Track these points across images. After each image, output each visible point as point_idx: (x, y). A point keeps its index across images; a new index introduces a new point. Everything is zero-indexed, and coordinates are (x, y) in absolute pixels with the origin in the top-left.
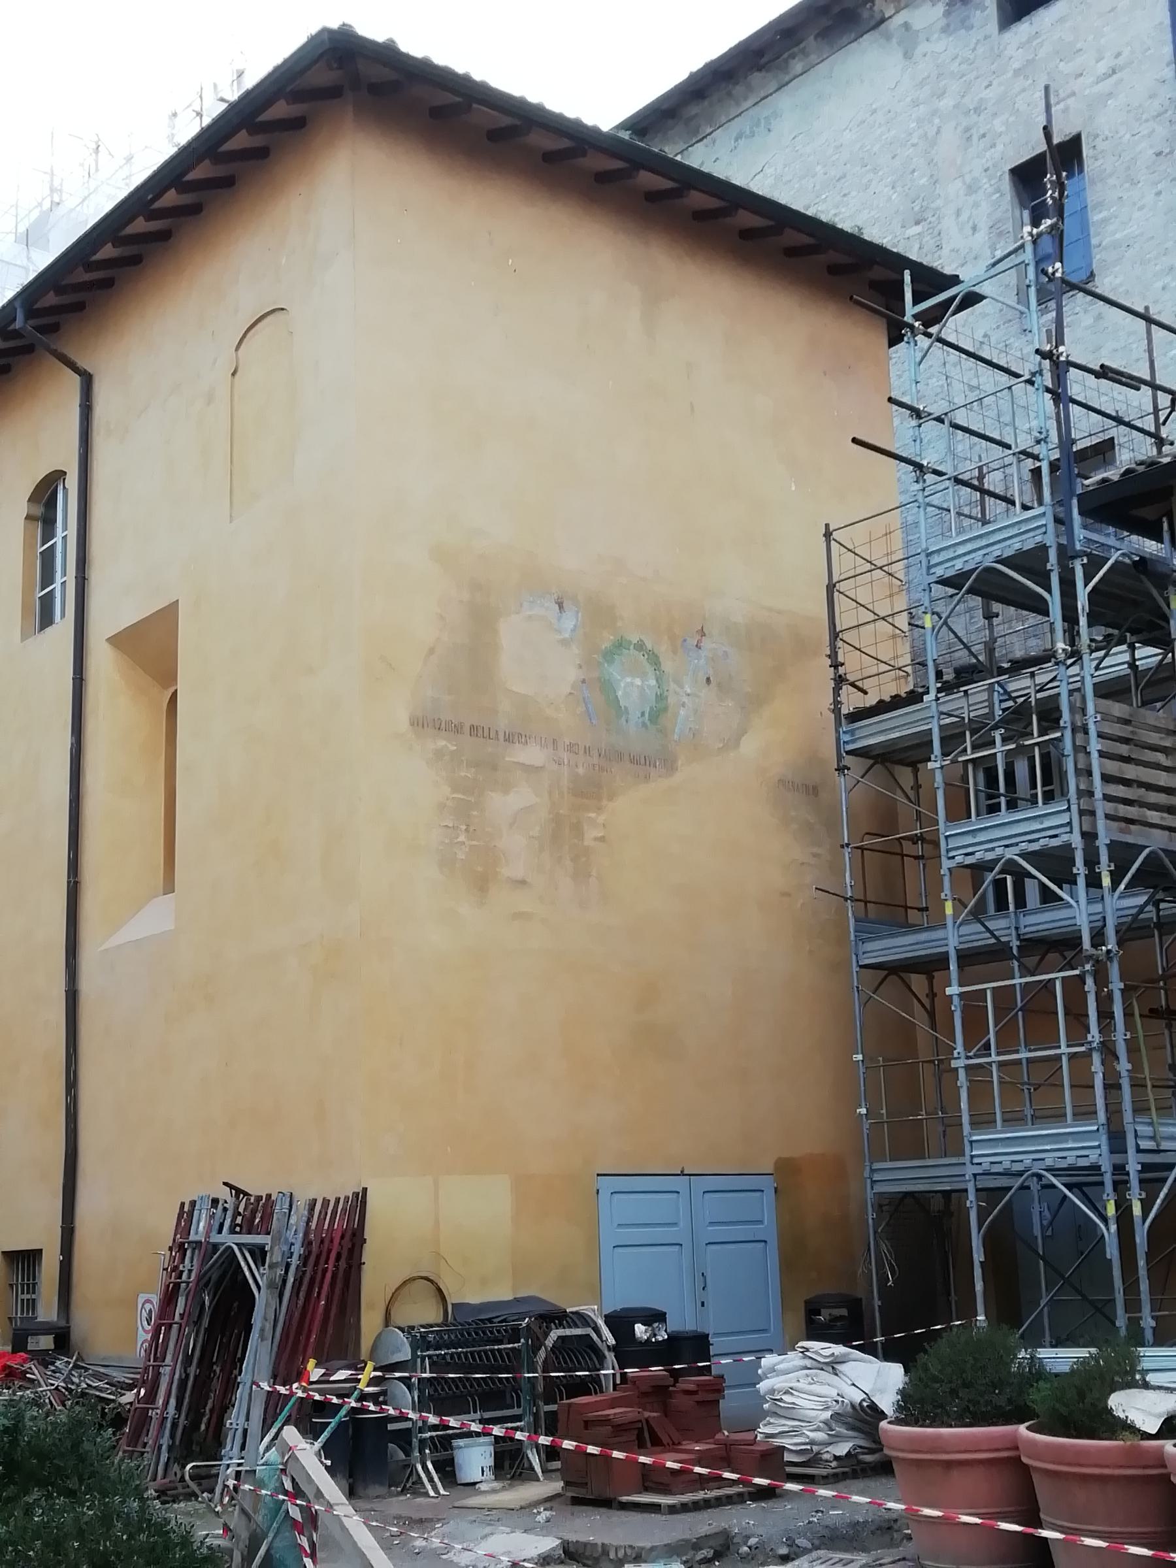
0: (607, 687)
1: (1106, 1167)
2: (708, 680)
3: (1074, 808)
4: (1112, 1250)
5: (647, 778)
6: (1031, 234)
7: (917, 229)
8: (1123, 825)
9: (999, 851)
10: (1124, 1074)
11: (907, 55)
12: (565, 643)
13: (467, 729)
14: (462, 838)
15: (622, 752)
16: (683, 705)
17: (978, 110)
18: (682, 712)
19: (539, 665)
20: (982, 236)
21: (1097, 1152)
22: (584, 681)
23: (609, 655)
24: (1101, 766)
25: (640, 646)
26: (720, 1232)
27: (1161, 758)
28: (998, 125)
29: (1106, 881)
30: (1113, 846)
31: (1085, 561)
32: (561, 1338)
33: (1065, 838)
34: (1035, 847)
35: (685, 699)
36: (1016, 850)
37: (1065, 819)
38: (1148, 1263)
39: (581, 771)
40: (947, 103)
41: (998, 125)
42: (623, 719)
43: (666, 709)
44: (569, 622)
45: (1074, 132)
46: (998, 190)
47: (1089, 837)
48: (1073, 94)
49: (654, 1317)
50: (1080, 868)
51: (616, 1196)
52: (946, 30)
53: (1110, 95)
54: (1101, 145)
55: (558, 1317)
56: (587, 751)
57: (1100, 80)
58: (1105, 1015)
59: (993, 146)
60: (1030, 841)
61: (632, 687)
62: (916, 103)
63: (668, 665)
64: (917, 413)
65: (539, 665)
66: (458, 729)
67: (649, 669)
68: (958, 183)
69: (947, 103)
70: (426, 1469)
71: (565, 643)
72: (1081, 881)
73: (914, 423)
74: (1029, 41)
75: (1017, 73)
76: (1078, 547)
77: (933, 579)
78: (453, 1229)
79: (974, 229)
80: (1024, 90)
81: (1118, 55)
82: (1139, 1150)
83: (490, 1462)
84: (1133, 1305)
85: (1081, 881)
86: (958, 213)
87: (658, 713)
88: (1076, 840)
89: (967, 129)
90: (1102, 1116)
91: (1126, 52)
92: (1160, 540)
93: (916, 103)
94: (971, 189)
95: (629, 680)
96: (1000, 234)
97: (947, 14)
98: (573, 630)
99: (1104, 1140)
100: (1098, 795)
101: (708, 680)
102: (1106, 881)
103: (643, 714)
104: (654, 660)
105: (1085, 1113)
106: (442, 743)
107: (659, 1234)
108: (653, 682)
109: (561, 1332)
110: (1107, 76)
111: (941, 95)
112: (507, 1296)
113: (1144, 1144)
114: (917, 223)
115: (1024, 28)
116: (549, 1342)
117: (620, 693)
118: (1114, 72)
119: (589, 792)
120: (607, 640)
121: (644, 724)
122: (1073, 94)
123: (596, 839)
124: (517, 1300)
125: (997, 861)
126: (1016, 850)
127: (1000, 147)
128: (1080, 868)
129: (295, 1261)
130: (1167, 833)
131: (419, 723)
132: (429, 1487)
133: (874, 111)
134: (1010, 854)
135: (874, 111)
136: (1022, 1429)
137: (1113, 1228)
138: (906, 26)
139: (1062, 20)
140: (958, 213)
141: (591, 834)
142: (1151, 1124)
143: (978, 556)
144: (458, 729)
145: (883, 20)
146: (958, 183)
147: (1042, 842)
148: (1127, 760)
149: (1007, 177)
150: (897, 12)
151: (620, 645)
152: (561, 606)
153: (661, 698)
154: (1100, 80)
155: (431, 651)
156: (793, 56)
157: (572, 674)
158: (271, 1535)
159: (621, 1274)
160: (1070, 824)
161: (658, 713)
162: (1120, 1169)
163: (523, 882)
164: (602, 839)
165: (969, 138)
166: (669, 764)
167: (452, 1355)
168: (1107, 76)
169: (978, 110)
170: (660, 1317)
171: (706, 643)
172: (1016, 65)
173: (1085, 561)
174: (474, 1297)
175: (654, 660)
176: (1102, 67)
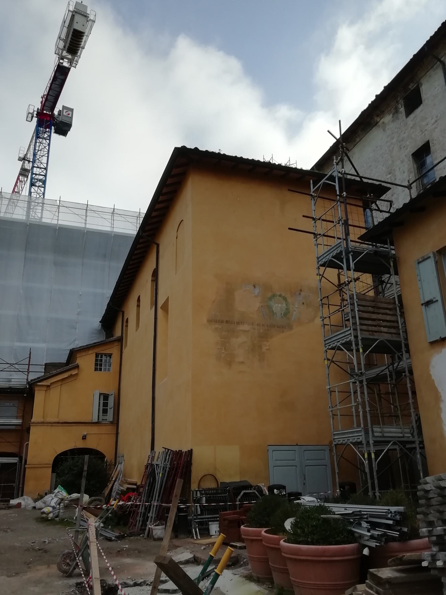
0: (270, 308)
1: (364, 442)
2: (303, 303)
3: (352, 329)
4: (367, 470)
5: (283, 332)
6: (336, 162)
7: (390, 175)
8: (371, 333)
9: (336, 344)
10: (368, 411)
11: (384, 130)
12: (256, 296)
13: (236, 323)
14: (223, 351)
15: (273, 325)
16: (295, 311)
17: (402, 140)
18: (295, 313)
19: (248, 303)
20: (406, 174)
21: (362, 438)
22: (262, 306)
23: (270, 299)
24: (359, 314)
25: (280, 296)
26: (279, 463)
27: (388, 312)
28: (408, 143)
29: (361, 350)
30: (363, 339)
31: (352, 253)
32: (244, 493)
33: (350, 338)
34: (343, 342)
35: (295, 309)
36: (339, 343)
37: (349, 332)
38: (377, 475)
39: (261, 331)
40: (395, 140)
41: (408, 143)
42: (275, 316)
43: (289, 312)
44: (257, 291)
45: (427, 140)
46: (409, 161)
47: (356, 337)
48: (426, 130)
49: (281, 487)
50: (354, 347)
51: (305, 452)
52: (393, 121)
53: (436, 128)
54: (434, 142)
55: (249, 487)
56: (263, 325)
57: (433, 125)
58: (362, 393)
59: (407, 149)
60: (342, 340)
61: (278, 307)
62: (387, 142)
63: (289, 300)
64: (314, 219)
65: (248, 303)
66: (222, 322)
67: (284, 302)
68: (399, 161)
69: (395, 140)
70: (196, 530)
71: (256, 296)
72: (354, 351)
73: (313, 222)
74: (414, 118)
75: (411, 128)
76: (350, 250)
77: (319, 265)
78: (220, 459)
79: (404, 172)
80: (413, 132)
81: (437, 117)
82: (373, 436)
83: (218, 529)
84: (373, 488)
85: (354, 351)
86: (400, 169)
87: (287, 313)
88: (352, 338)
89: (400, 146)
90: (362, 426)
91: (439, 115)
92: (387, 245)
93: (387, 142)
94: (402, 162)
95: (277, 305)
96: (411, 172)
97: (393, 117)
98: (258, 293)
99: (363, 433)
100: (358, 324)
101: (303, 303)
102: (361, 350)
103: (281, 314)
104: (285, 299)
105: (359, 425)
106: (217, 326)
107: (291, 463)
108: (285, 305)
109: (245, 491)
110: (434, 123)
111: (393, 138)
112: (238, 480)
113: (376, 434)
114: (390, 174)
115: (412, 116)
116: (242, 493)
117: (274, 309)
118: (436, 122)
119: (264, 336)
120: (269, 295)
121: (282, 317)
122: (426, 130)
123: (266, 349)
124: (241, 481)
125: (335, 347)
126: (339, 343)
127: (409, 149)
128: (354, 347)
129: (167, 469)
130: (390, 335)
131: (210, 321)
132: (195, 536)
133: (377, 147)
134: (338, 344)
135: (377, 147)
136: (263, 531)
137: (367, 462)
138: (383, 123)
139: (422, 111)
140: (400, 169)
141: (264, 349)
142: (380, 428)
143: (328, 257)
144: (222, 322)
145: (378, 123)
146: (399, 161)
147: (345, 340)
148: (374, 313)
149: (411, 157)
150: (380, 120)
151: (274, 296)
152: (255, 287)
153: (287, 309)
154: (433, 125)
155: (214, 302)
156: (356, 137)
157: (258, 305)
158: (83, 550)
159: (280, 473)
160: (351, 333)
161: (287, 313)
162: (368, 442)
163: (243, 362)
164: (268, 349)
165: (401, 148)
166: (290, 327)
167: (213, 497)
168: (434, 123)
169: (402, 140)
170: (284, 487)
171: (303, 293)
172: (411, 126)
173: (352, 253)
174: (227, 480)
175: (285, 299)
176: (433, 121)
